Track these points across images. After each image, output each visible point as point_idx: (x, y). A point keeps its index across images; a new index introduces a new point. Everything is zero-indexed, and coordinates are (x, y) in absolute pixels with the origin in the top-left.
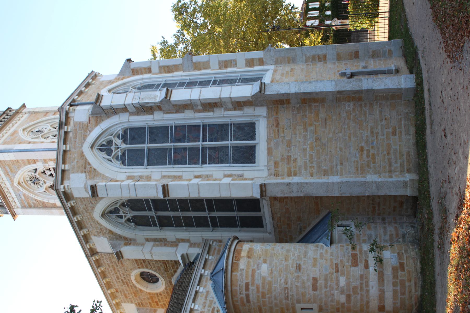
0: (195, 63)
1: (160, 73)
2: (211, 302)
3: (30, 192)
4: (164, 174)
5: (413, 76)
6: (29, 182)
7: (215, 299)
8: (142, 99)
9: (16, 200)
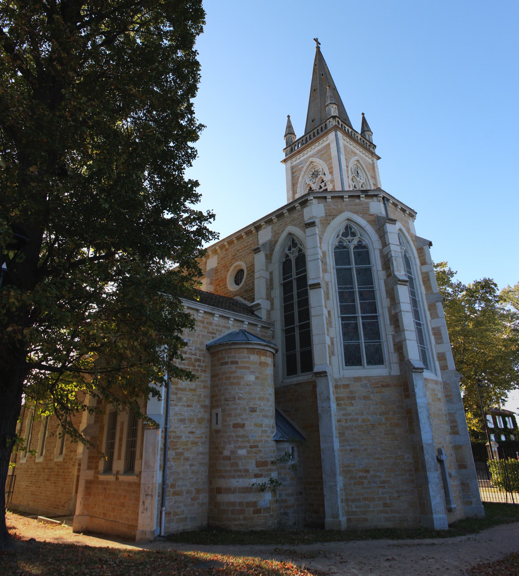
0: (435, 305)
1: (422, 273)
2: (221, 331)
3: (305, 172)
4: (330, 284)
5: (446, 528)
6: (313, 170)
7: (223, 335)
8: (396, 259)
9: (298, 161)
